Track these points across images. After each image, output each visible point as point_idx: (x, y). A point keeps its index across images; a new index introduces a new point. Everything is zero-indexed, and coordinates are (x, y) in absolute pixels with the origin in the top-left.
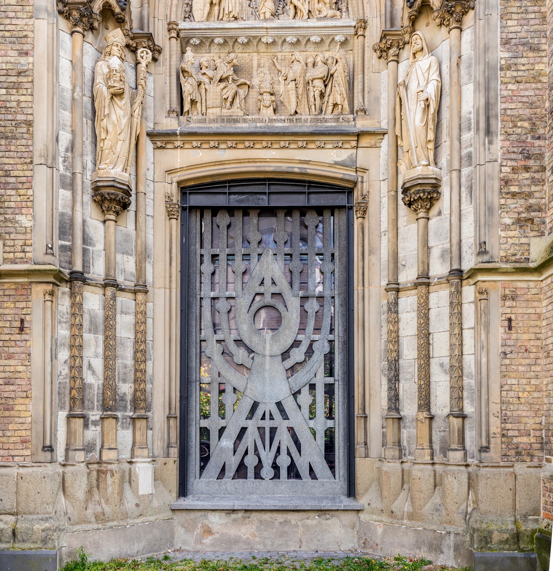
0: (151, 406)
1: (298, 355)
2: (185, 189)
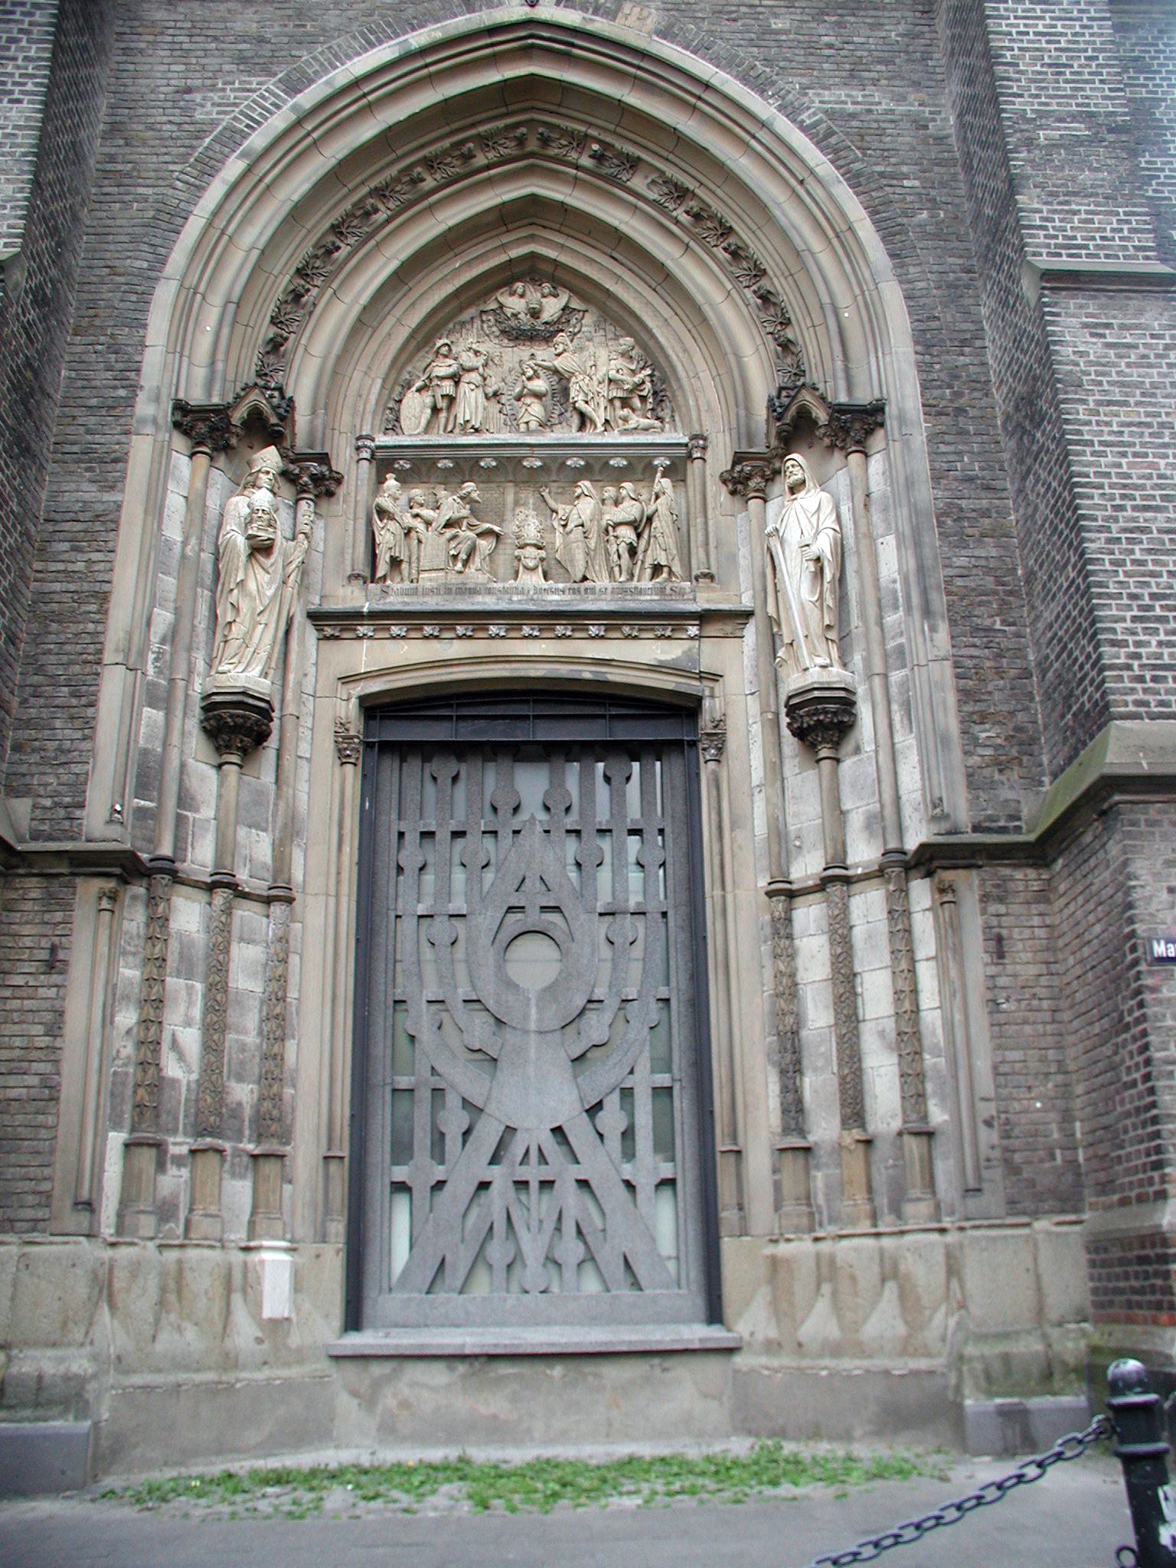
0: (290, 1133)
1: (596, 1027)
2: (374, 708)
